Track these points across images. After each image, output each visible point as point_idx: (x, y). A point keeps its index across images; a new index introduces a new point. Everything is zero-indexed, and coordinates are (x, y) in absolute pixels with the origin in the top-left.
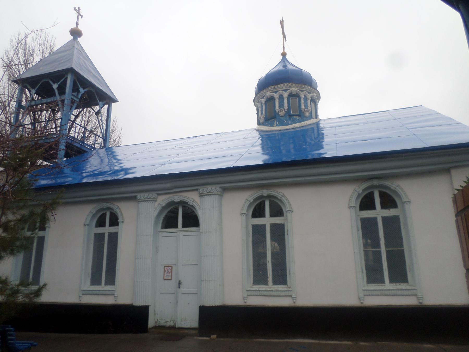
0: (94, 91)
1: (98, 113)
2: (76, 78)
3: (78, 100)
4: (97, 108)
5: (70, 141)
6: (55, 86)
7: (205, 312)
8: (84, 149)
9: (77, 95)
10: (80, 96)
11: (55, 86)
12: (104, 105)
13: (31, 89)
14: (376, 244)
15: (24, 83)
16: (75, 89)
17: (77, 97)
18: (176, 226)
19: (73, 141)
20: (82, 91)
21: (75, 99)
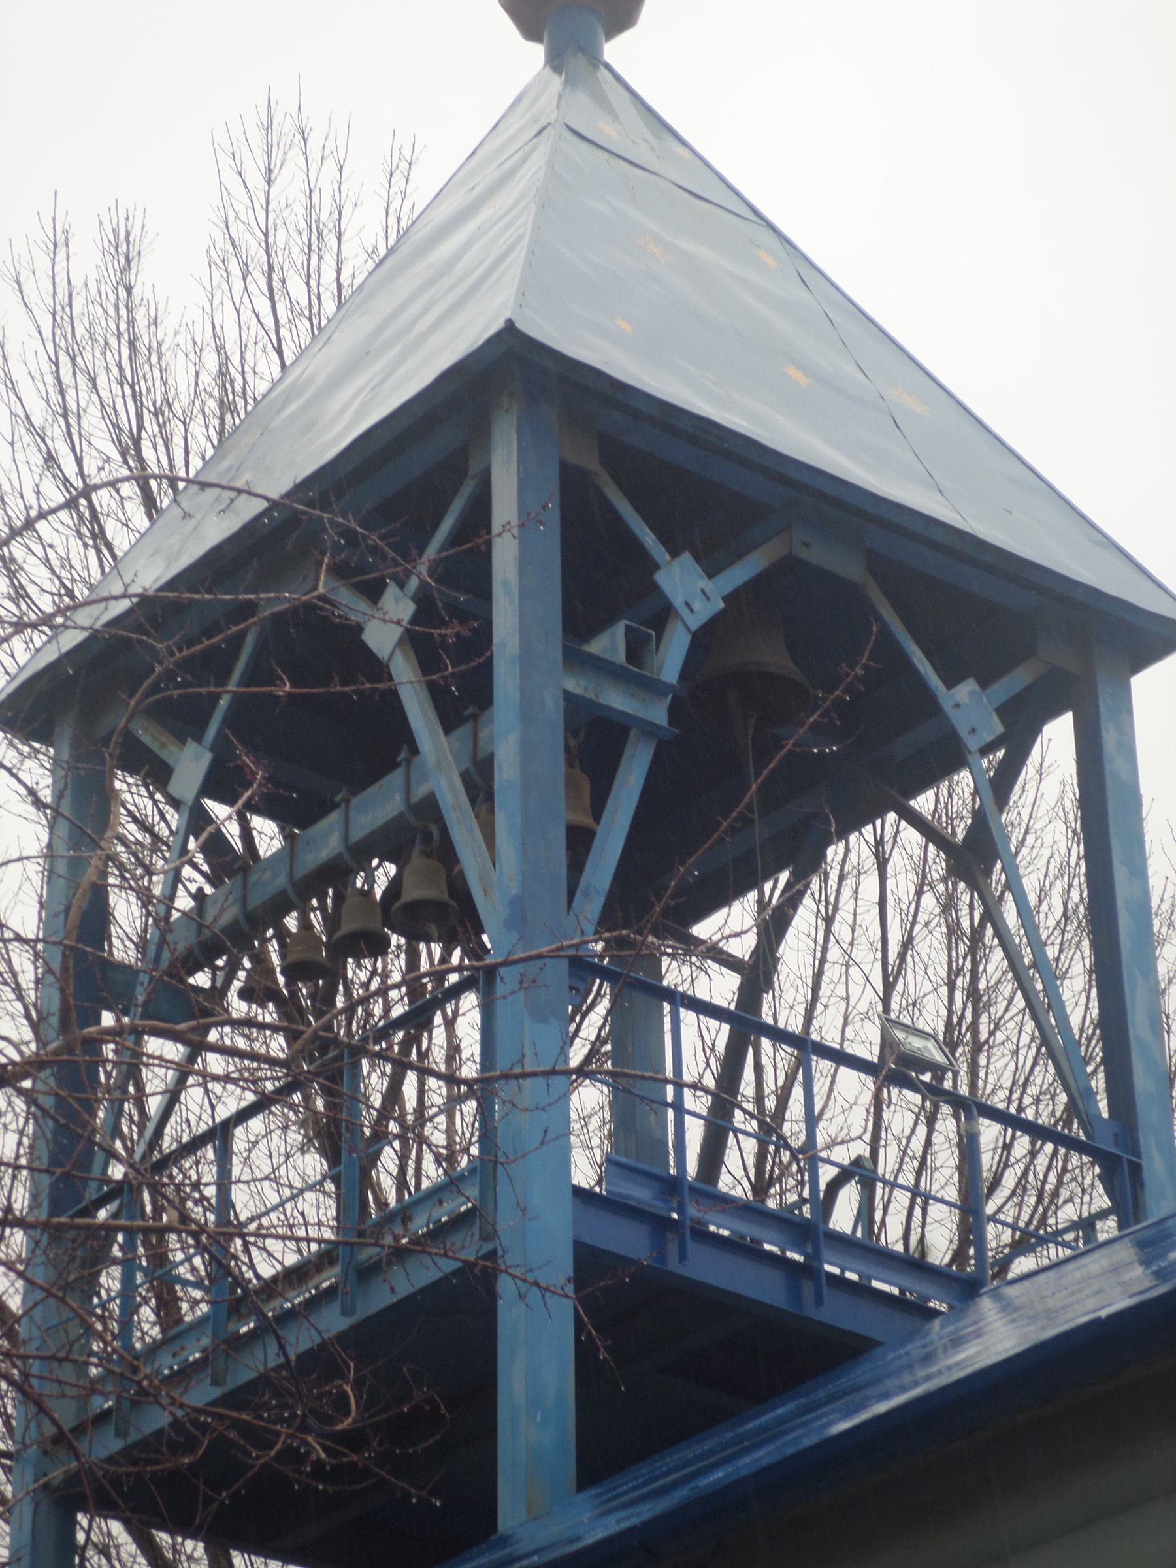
0: (846, 565)
1: (975, 856)
2: (591, 462)
3: (658, 714)
4: (952, 798)
5: (628, 1241)
6: (384, 628)
7: (724, 599)
8: (836, 1313)
9: (636, 649)
10: (671, 659)
11: (384, 628)
12: (1018, 741)
13: (169, 752)
14: (779, 1422)
15: (99, 702)
16: (600, 583)
17: (634, 671)
18: (424, 674)
19: (809, 1270)
20: (692, 590)
21: (617, 700)
